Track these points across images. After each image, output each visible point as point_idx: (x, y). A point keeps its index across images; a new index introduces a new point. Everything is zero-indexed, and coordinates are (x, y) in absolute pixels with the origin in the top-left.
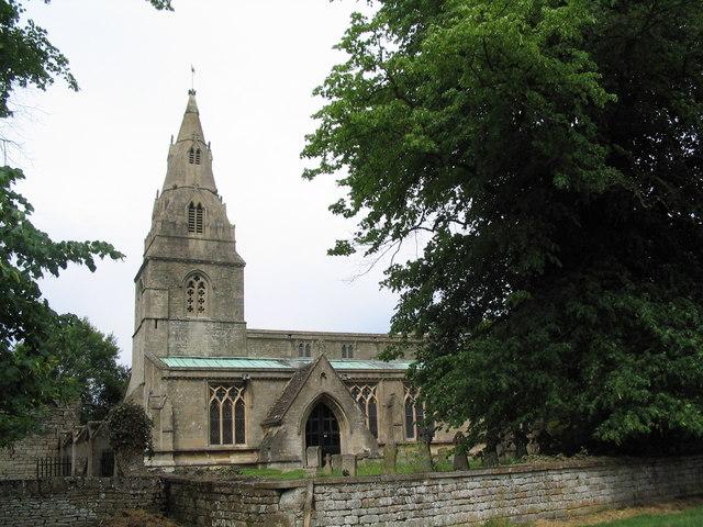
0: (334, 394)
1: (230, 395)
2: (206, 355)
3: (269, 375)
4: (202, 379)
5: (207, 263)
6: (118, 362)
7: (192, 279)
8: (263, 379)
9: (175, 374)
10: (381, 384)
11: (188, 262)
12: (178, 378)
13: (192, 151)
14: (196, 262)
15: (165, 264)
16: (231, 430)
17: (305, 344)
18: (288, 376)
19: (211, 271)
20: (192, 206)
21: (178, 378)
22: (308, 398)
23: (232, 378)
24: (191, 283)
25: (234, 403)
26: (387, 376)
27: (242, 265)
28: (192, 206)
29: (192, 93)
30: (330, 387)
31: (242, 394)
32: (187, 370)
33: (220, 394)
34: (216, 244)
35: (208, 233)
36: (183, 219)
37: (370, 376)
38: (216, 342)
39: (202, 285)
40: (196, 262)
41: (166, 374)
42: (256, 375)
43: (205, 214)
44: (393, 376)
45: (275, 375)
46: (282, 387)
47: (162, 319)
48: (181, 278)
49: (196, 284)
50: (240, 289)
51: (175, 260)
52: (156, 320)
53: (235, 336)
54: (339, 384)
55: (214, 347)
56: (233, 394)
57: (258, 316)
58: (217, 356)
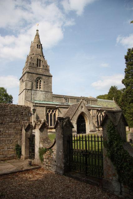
0: (84, 112)
1: (52, 112)
2: (42, 100)
3: (63, 106)
4: (44, 106)
5: (43, 75)
6: (119, 89)
7: (38, 79)
8: (61, 107)
9: (37, 105)
10: (91, 110)
11: (37, 74)
12: (38, 106)
13: (38, 45)
14: (39, 74)
15: (31, 74)
16: (52, 122)
17: (68, 99)
18: (68, 107)
19: (44, 77)
20: (38, 59)
21: (38, 106)
22: (79, 113)
23: (53, 107)
24: (38, 80)
25: (53, 114)
26: (93, 108)
27: (51, 76)
28: (38, 59)
29: (37, 30)
30: (84, 110)
31: (55, 112)
32: (40, 104)
33: (49, 111)
34: (44, 70)
35: (41, 67)
36: (35, 62)
37: (103, 109)
38: (44, 97)
39: (41, 81)
40: (39, 74)
41: (34, 104)
42: (60, 106)
43: (41, 62)
44: (94, 108)
45: (65, 107)
46: (59, 109)
47: (30, 90)
48: (35, 79)
49: (39, 81)
50: (51, 83)
51: (33, 73)
52: (28, 90)
53: (49, 95)
54: (86, 110)
55: (44, 98)
56: (53, 111)
57: (56, 91)
58: (45, 101)
